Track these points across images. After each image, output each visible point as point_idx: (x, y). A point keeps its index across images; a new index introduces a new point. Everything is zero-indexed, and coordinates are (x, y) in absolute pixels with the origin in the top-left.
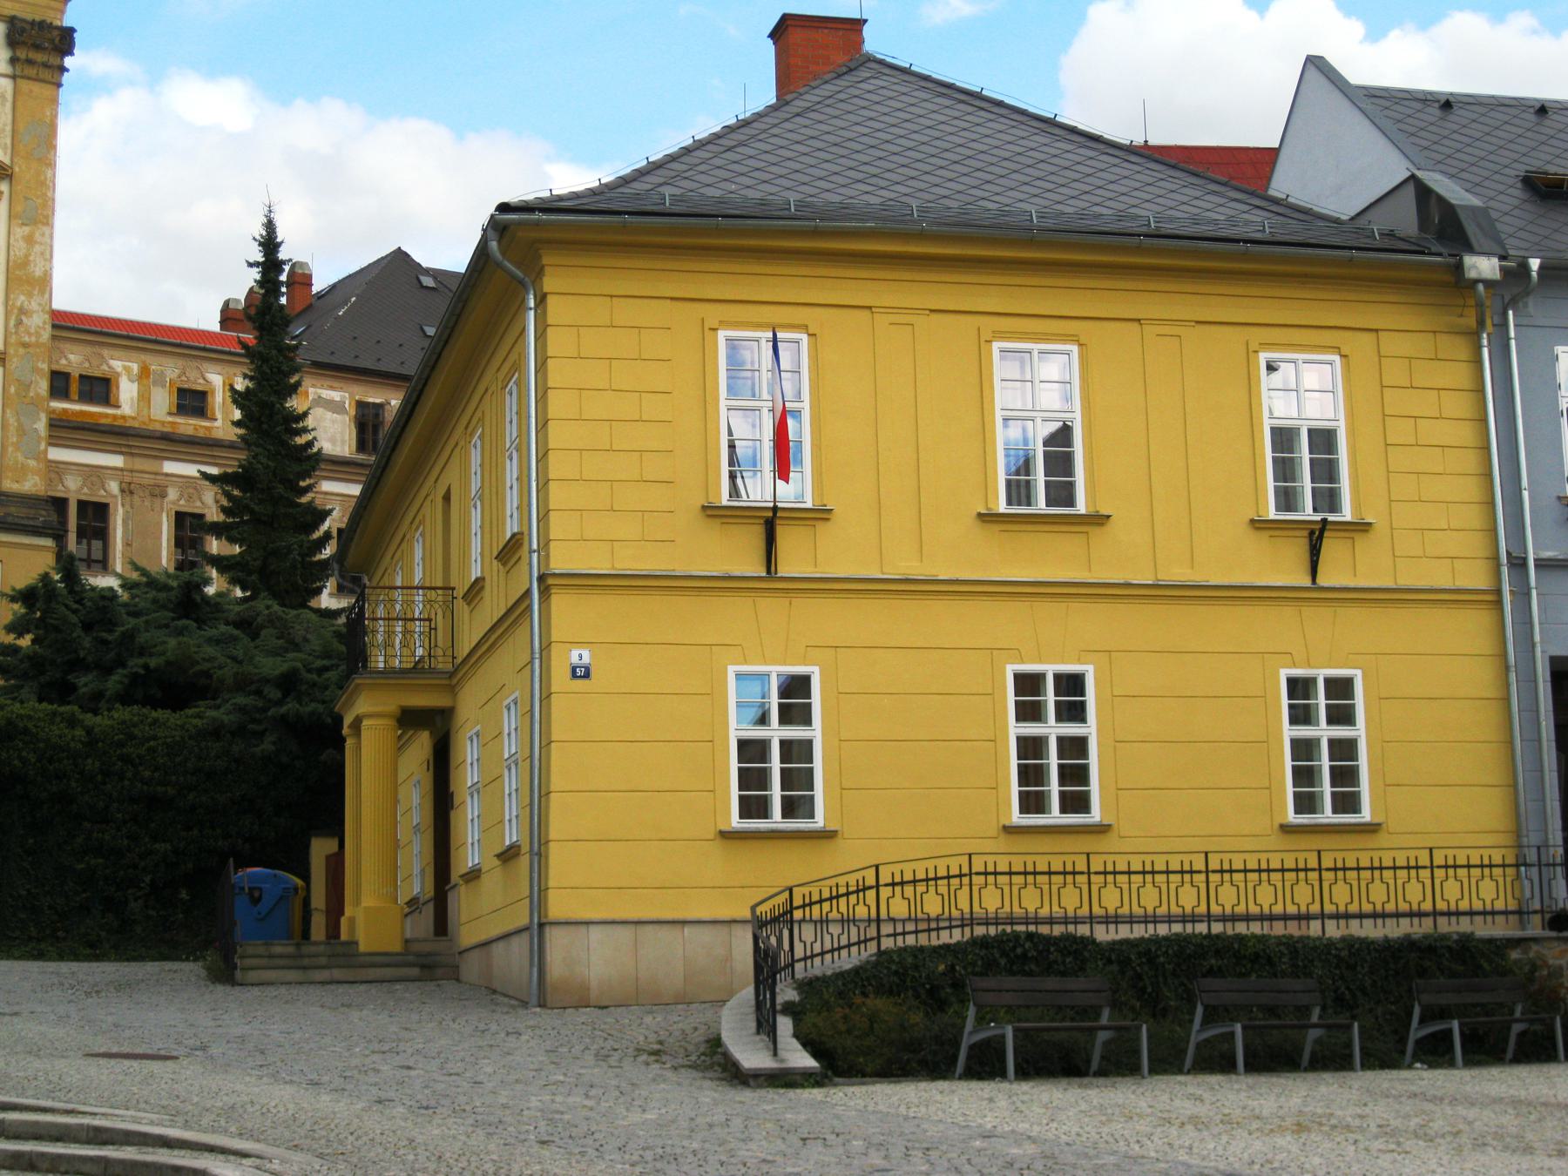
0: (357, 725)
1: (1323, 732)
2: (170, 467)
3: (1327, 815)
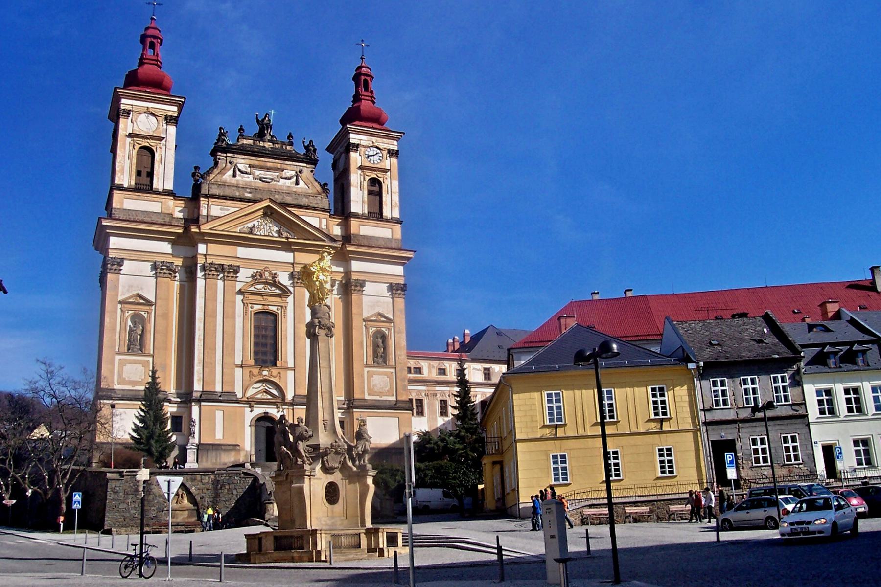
0: (485, 464)
1: (666, 458)
2: (437, 388)
3: (668, 475)
